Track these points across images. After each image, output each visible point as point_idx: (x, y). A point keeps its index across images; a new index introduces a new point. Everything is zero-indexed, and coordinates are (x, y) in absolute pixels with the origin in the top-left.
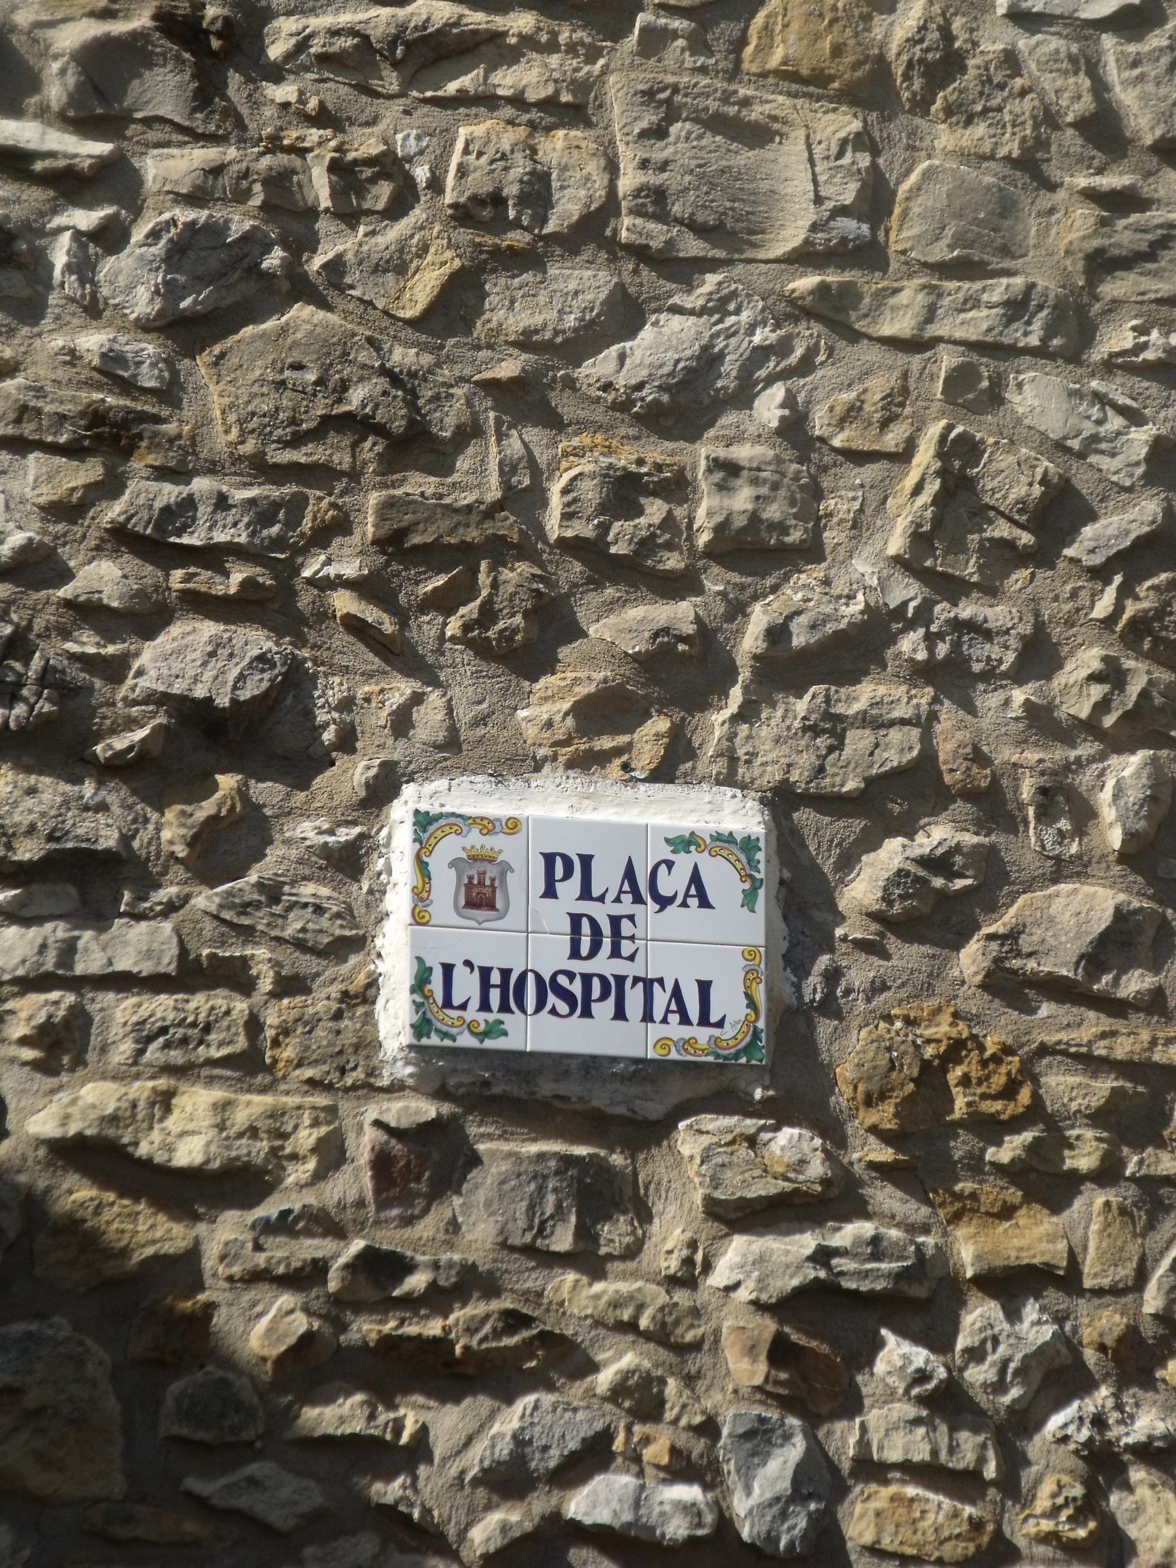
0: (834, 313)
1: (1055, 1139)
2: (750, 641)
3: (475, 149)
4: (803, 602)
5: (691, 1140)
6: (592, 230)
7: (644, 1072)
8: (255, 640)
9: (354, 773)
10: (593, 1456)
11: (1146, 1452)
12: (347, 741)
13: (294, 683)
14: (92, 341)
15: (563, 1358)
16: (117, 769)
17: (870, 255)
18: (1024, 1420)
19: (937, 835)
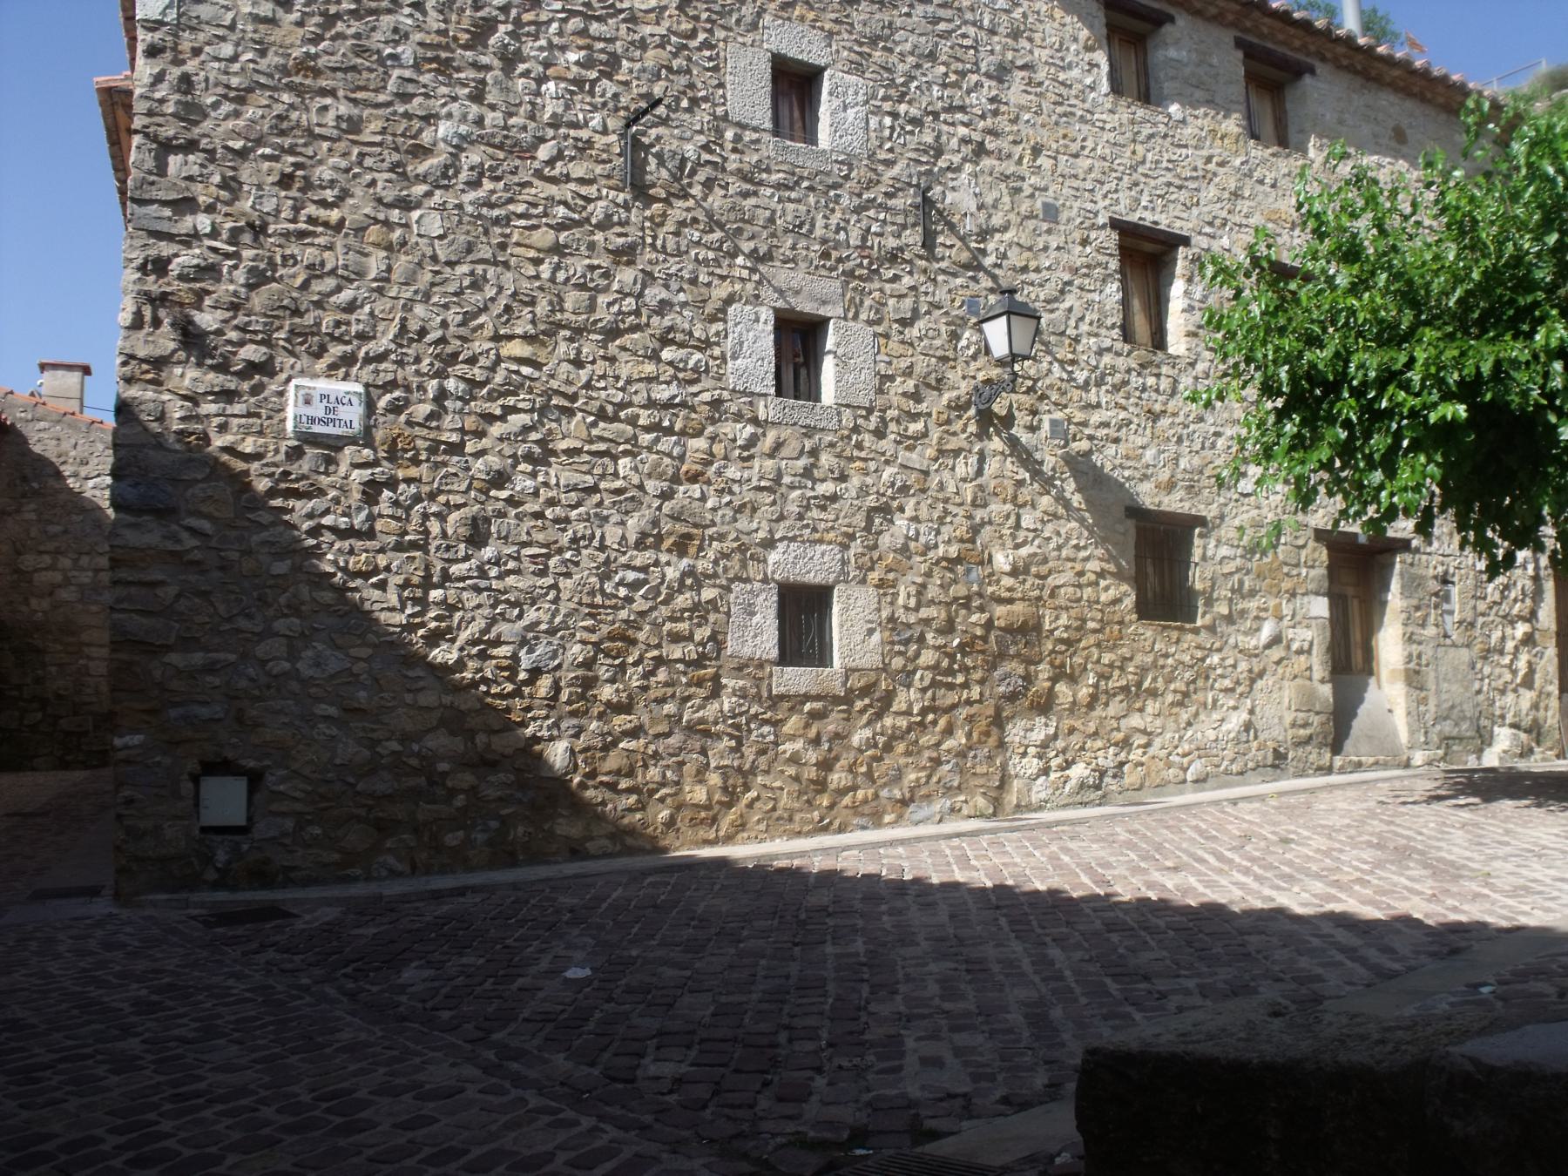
0: (380, 291)
1: (418, 454)
2: (362, 354)
3: (309, 254)
4: (373, 347)
5: (348, 450)
6: (333, 272)
7: (338, 437)
8: (264, 349)
9: (283, 376)
10: (327, 512)
11: (433, 514)
12: (281, 370)
13: (271, 358)
14: (231, 288)
15: (321, 492)
16: (235, 374)
17: (388, 280)
18: (410, 507)
19: (397, 394)
